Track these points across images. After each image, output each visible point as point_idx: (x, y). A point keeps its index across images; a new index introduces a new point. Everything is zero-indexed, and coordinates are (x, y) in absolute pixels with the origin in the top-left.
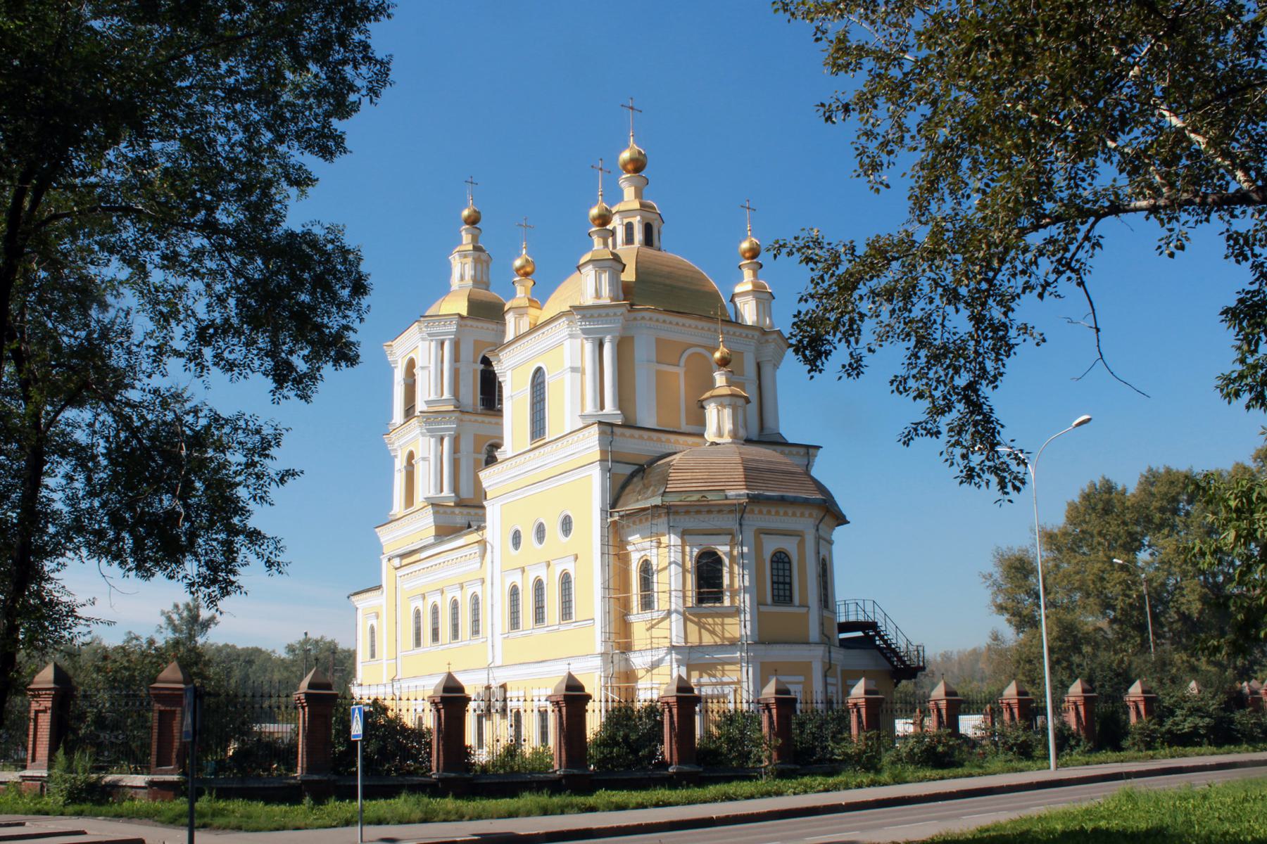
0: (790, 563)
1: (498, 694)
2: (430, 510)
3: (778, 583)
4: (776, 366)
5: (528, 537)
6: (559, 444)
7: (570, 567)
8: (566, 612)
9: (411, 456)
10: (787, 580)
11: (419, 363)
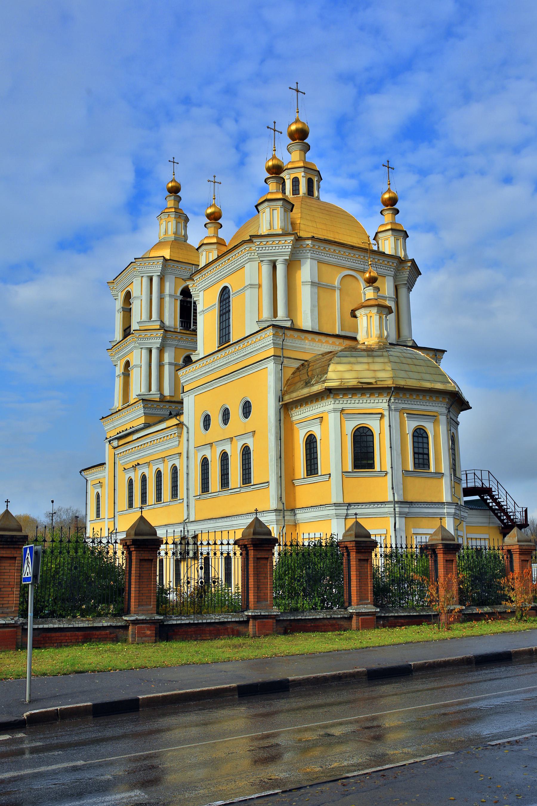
0: (427, 438)
1: (256, 743)
2: (141, 405)
3: (423, 454)
4: (410, 289)
5: (216, 419)
6: (241, 345)
7: (250, 442)
8: (246, 478)
9: (128, 364)
10: (416, 456)
11: (133, 295)
